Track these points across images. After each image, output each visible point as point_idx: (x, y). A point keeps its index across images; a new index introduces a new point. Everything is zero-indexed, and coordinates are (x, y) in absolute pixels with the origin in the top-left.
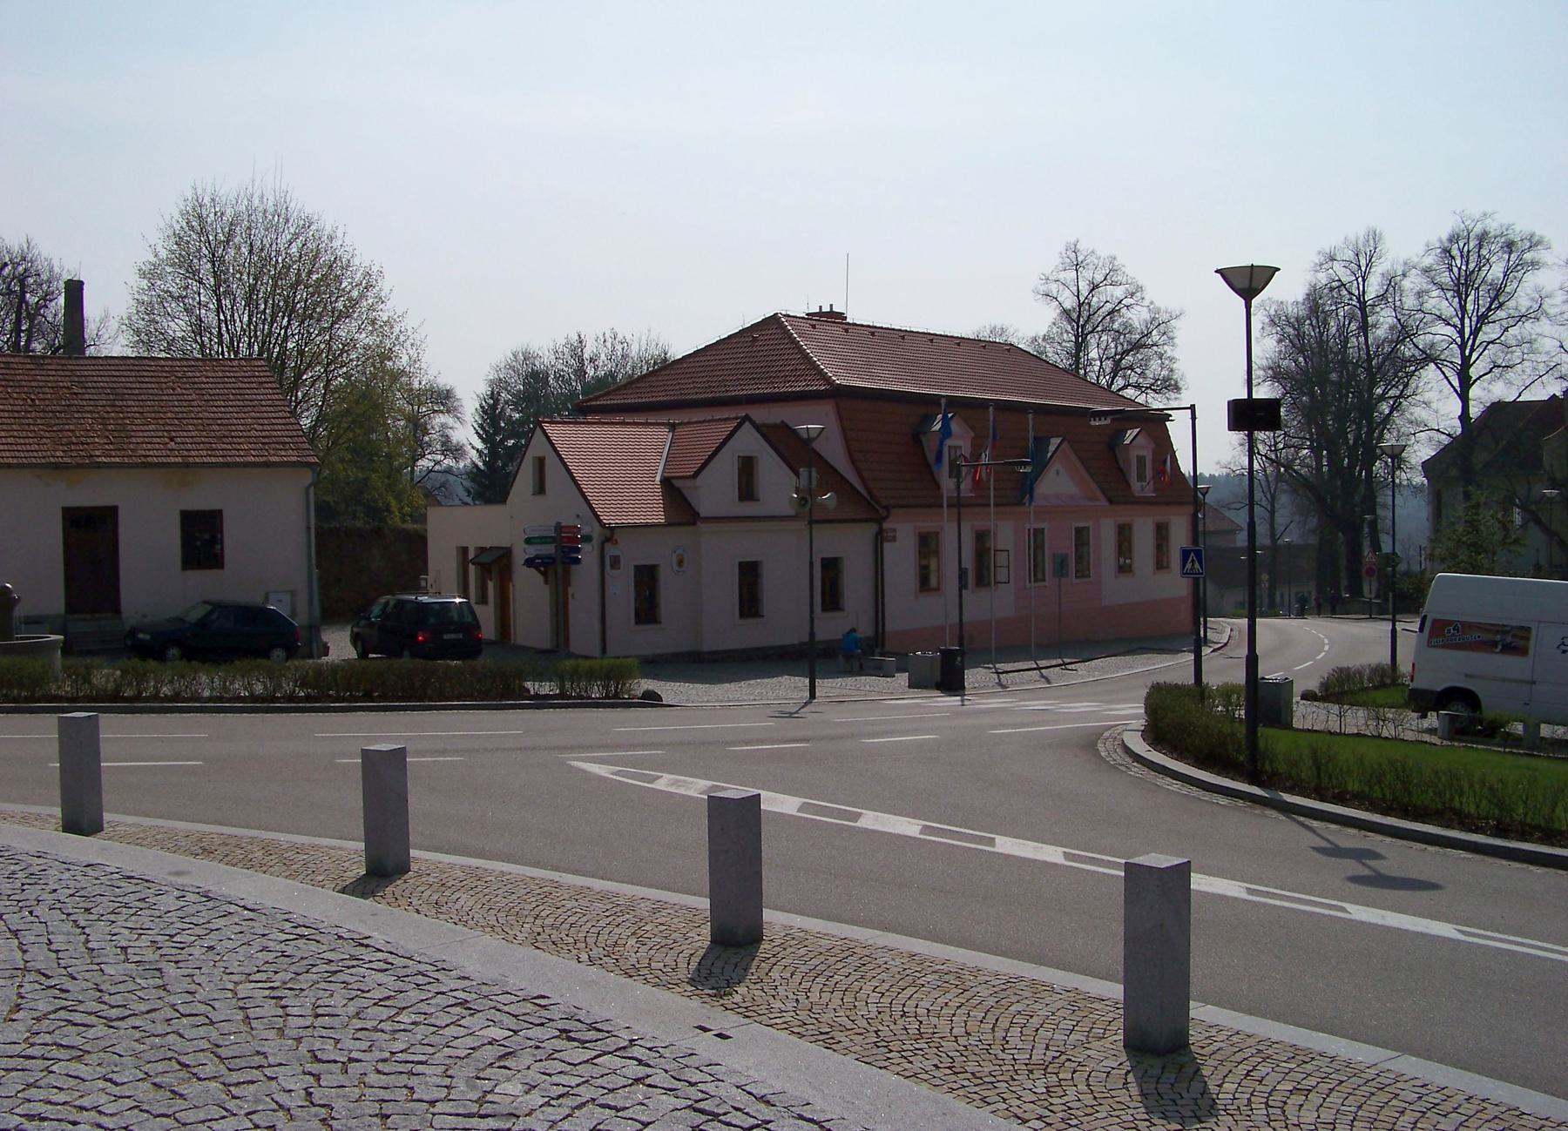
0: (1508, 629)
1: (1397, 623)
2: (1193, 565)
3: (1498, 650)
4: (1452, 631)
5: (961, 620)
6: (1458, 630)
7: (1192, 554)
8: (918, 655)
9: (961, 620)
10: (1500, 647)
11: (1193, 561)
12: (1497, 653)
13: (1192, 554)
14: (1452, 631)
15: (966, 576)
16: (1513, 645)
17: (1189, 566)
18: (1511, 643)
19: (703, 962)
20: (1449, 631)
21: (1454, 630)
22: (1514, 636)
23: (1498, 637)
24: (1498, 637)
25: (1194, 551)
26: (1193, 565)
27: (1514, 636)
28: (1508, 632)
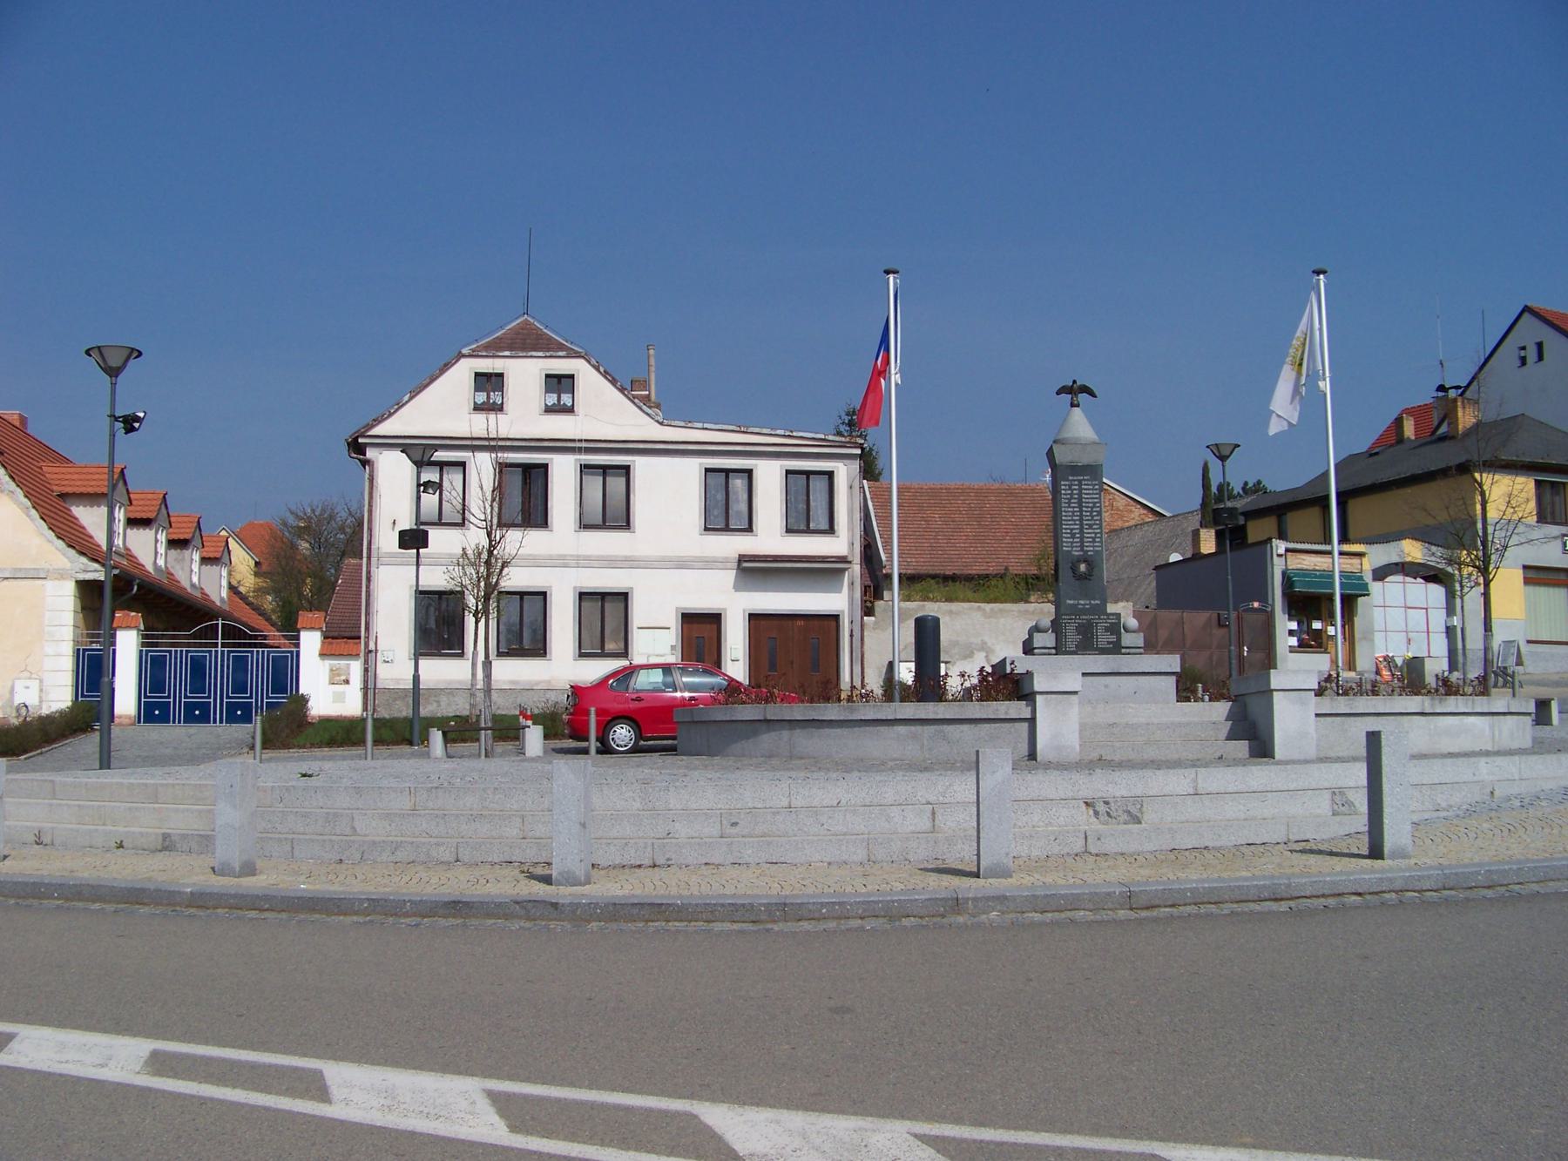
5: (416, 678)
9: (416, 678)
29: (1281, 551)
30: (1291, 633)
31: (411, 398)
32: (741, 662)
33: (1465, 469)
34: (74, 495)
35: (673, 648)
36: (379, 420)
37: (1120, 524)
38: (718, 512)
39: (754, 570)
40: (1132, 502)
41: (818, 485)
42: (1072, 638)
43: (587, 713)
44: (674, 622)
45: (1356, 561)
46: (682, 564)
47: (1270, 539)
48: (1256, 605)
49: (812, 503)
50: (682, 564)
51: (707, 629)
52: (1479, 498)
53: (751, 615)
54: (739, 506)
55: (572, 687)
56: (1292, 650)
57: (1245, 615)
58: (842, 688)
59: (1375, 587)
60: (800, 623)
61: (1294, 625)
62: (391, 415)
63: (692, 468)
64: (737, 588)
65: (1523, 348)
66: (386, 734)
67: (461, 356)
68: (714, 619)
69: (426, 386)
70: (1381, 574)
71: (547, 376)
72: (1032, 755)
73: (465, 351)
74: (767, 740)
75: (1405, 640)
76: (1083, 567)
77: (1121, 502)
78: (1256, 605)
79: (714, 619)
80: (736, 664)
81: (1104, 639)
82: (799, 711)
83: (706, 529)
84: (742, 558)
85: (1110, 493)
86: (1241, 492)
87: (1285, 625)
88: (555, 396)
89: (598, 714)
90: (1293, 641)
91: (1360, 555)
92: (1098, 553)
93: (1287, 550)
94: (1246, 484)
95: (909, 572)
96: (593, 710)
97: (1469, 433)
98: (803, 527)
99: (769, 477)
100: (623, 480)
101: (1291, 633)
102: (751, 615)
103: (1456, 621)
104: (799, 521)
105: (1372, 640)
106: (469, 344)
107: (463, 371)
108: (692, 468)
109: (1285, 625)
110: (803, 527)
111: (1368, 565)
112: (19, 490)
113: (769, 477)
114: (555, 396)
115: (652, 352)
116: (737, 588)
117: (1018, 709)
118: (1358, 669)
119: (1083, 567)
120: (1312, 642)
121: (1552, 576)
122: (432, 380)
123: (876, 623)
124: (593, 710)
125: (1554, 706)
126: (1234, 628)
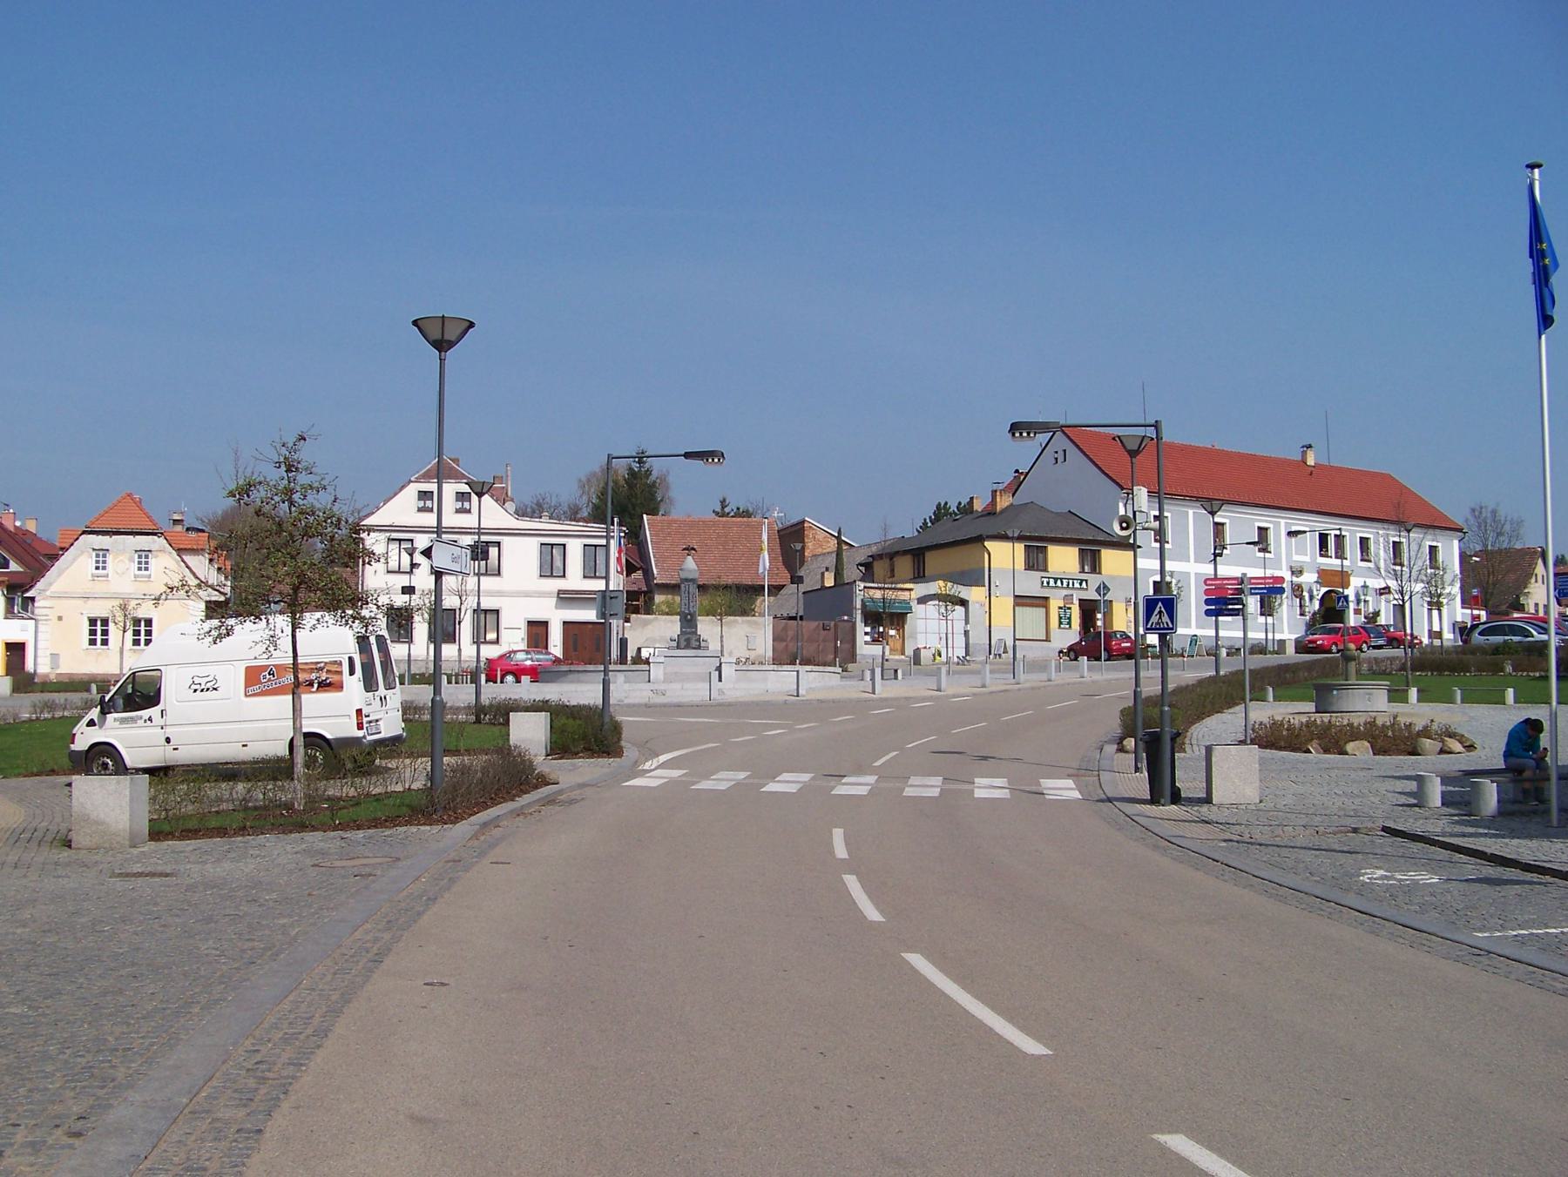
0: (322, 665)
1: (298, 630)
2: (1160, 618)
3: (314, 689)
4: (268, 676)
5: (409, 655)
6: (273, 674)
7: (1160, 604)
8: (20, 561)
9: (409, 655)
10: (316, 686)
11: (1160, 612)
12: (313, 692)
13: (1160, 604)
14: (268, 676)
15: (1056, 667)
16: (328, 681)
17: (1154, 619)
18: (327, 679)
19: (554, 725)
20: (265, 677)
21: (269, 674)
22: (328, 671)
23: (313, 676)
24: (313, 676)
25: (1163, 601)
26: (1160, 618)
27: (328, 671)
28: (321, 669)
29: (862, 587)
30: (866, 634)
31: (384, 504)
32: (559, 647)
33: (980, 539)
34: (185, 549)
35: (523, 639)
36: (368, 516)
37: (819, 551)
38: (548, 567)
39: (567, 598)
40: (829, 535)
41: (601, 553)
42: (683, 644)
43: (497, 671)
44: (524, 626)
45: (907, 593)
46: (527, 595)
47: (855, 581)
48: (846, 618)
49: (598, 562)
50: (527, 595)
51: (541, 629)
52: (986, 556)
53: (564, 622)
54: (558, 563)
55: (487, 659)
56: (866, 643)
57: (839, 623)
58: (310, 618)
59: (919, 610)
60: (590, 626)
61: (868, 629)
62: (373, 513)
63: (534, 543)
64: (556, 608)
65: (1056, 452)
66: (1397, 545)
67: (410, 481)
68: (545, 624)
69: (392, 498)
70: (923, 600)
71: (457, 493)
72: (649, 681)
73: (413, 479)
74: (571, 676)
75: (938, 638)
76: (689, 617)
77: (821, 535)
78: (846, 618)
79: (545, 624)
80: (556, 645)
81: (694, 644)
82: (581, 668)
83: (541, 576)
84: (560, 592)
85: (814, 529)
86: (956, 510)
87: (862, 629)
88: (460, 503)
89: (501, 670)
90: (868, 638)
91: (910, 590)
92: (695, 612)
93: (865, 587)
94: (960, 503)
95: (673, 582)
96: (499, 669)
97: (1004, 511)
98: (593, 575)
99: (575, 548)
100: (497, 549)
101: (866, 634)
102: (564, 622)
103: (969, 627)
104: (590, 572)
105: (916, 638)
106: (415, 474)
107: (412, 490)
108: (534, 543)
109: (862, 629)
110: (593, 575)
111: (914, 595)
112: (679, 623)
113: (575, 548)
114: (460, 503)
115: (509, 468)
116: (556, 608)
117: (645, 667)
118: (906, 654)
119: (689, 617)
120: (877, 639)
121: (1034, 601)
122: (396, 494)
123: (631, 627)
124: (499, 669)
125: (899, 672)
126: (833, 630)
